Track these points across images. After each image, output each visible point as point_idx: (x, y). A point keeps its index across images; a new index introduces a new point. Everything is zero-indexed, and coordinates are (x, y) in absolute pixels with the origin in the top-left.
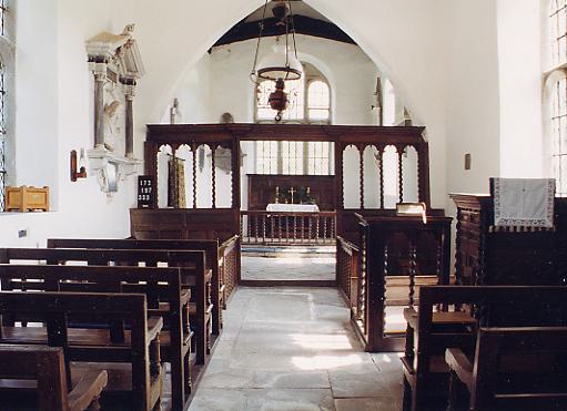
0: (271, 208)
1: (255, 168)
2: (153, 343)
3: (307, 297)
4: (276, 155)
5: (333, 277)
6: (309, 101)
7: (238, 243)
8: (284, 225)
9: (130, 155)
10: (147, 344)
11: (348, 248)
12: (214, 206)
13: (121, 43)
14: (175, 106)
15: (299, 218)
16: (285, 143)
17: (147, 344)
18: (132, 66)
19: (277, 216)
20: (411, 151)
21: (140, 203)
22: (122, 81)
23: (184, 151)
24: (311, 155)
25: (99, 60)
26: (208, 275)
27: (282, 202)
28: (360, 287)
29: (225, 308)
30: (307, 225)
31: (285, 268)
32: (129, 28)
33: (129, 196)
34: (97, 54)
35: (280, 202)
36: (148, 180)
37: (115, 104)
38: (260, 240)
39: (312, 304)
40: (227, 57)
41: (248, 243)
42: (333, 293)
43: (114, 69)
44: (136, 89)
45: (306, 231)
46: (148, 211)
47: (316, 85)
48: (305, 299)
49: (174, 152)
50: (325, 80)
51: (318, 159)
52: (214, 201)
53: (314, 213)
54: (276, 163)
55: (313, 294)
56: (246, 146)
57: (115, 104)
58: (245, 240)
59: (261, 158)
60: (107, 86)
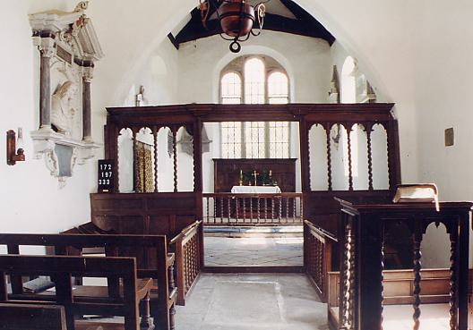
0: (236, 190)
1: (221, 153)
2: (143, 302)
3: (273, 286)
4: (239, 141)
5: (300, 262)
6: (269, 90)
7: (200, 229)
8: (248, 206)
9: (88, 139)
10: (137, 302)
11: (319, 235)
12: (176, 189)
13: (74, 18)
14: (141, 93)
15: (262, 200)
16: (248, 124)
17: (137, 302)
18: (89, 47)
19: (240, 197)
20: (379, 130)
21: (101, 187)
22: (77, 62)
23: (145, 135)
24: (262, 146)
25: (44, 34)
26: (170, 260)
27: (245, 184)
28: (343, 288)
29: (181, 302)
30: (269, 205)
31: (256, 251)
32: (82, 6)
33: (86, 178)
34: (43, 28)
35: (243, 185)
36: (108, 165)
37: (67, 84)
38: (225, 220)
39: (280, 298)
40: (194, 51)
41: (208, 224)
42: (301, 281)
43: (63, 44)
44: (94, 72)
45: (270, 211)
46: (108, 196)
47: (277, 76)
48: (271, 289)
49: (134, 135)
50: (283, 70)
51: (280, 140)
52: (175, 185)
53: (277, 195)
54: (240, 148)
55: (281, 283)
56: (210, 128)
57: (67, 84)
58: (205, 220)
59: (226, 140)
60: (55, 65)
